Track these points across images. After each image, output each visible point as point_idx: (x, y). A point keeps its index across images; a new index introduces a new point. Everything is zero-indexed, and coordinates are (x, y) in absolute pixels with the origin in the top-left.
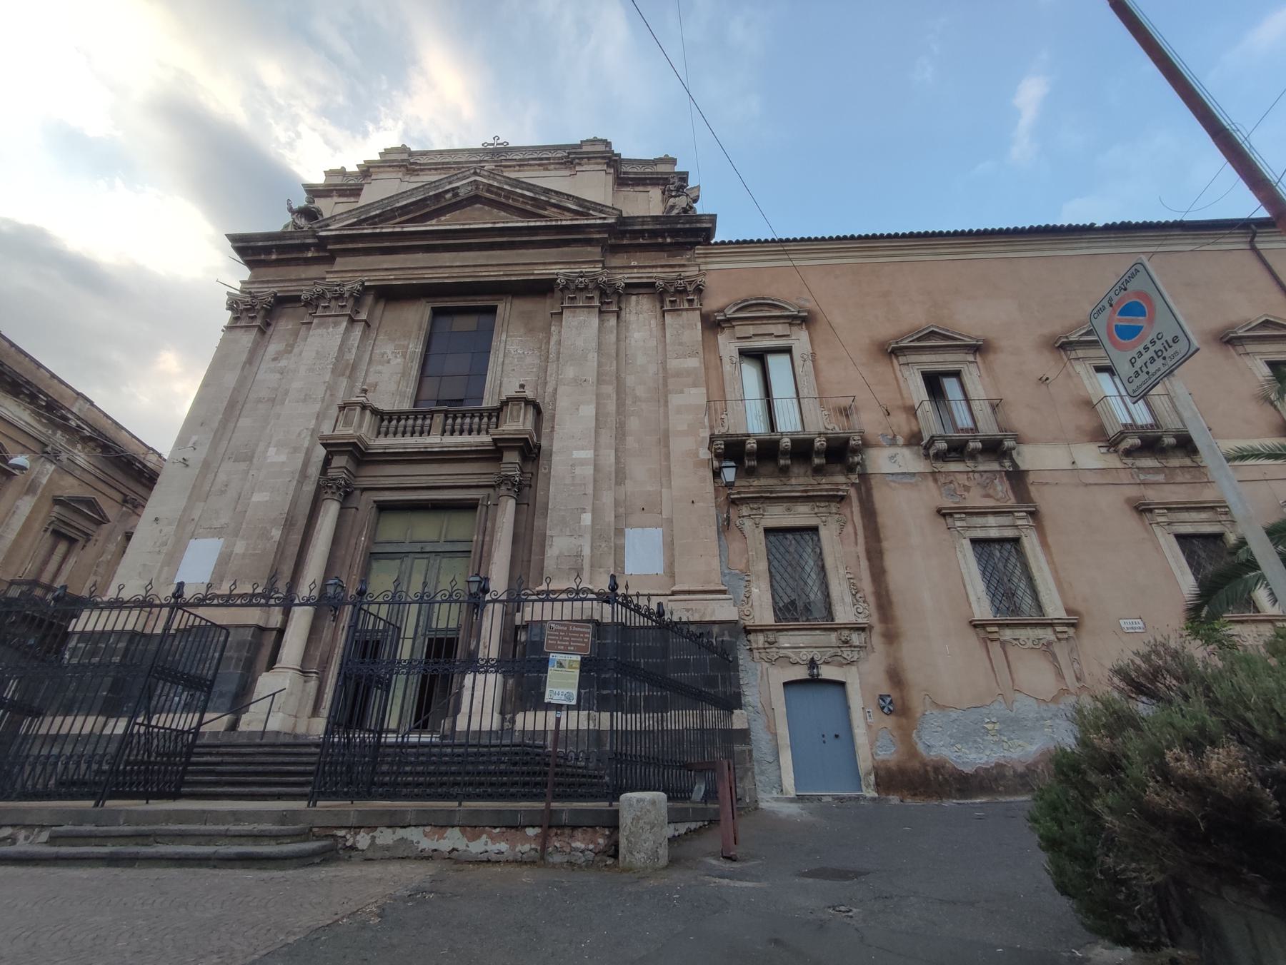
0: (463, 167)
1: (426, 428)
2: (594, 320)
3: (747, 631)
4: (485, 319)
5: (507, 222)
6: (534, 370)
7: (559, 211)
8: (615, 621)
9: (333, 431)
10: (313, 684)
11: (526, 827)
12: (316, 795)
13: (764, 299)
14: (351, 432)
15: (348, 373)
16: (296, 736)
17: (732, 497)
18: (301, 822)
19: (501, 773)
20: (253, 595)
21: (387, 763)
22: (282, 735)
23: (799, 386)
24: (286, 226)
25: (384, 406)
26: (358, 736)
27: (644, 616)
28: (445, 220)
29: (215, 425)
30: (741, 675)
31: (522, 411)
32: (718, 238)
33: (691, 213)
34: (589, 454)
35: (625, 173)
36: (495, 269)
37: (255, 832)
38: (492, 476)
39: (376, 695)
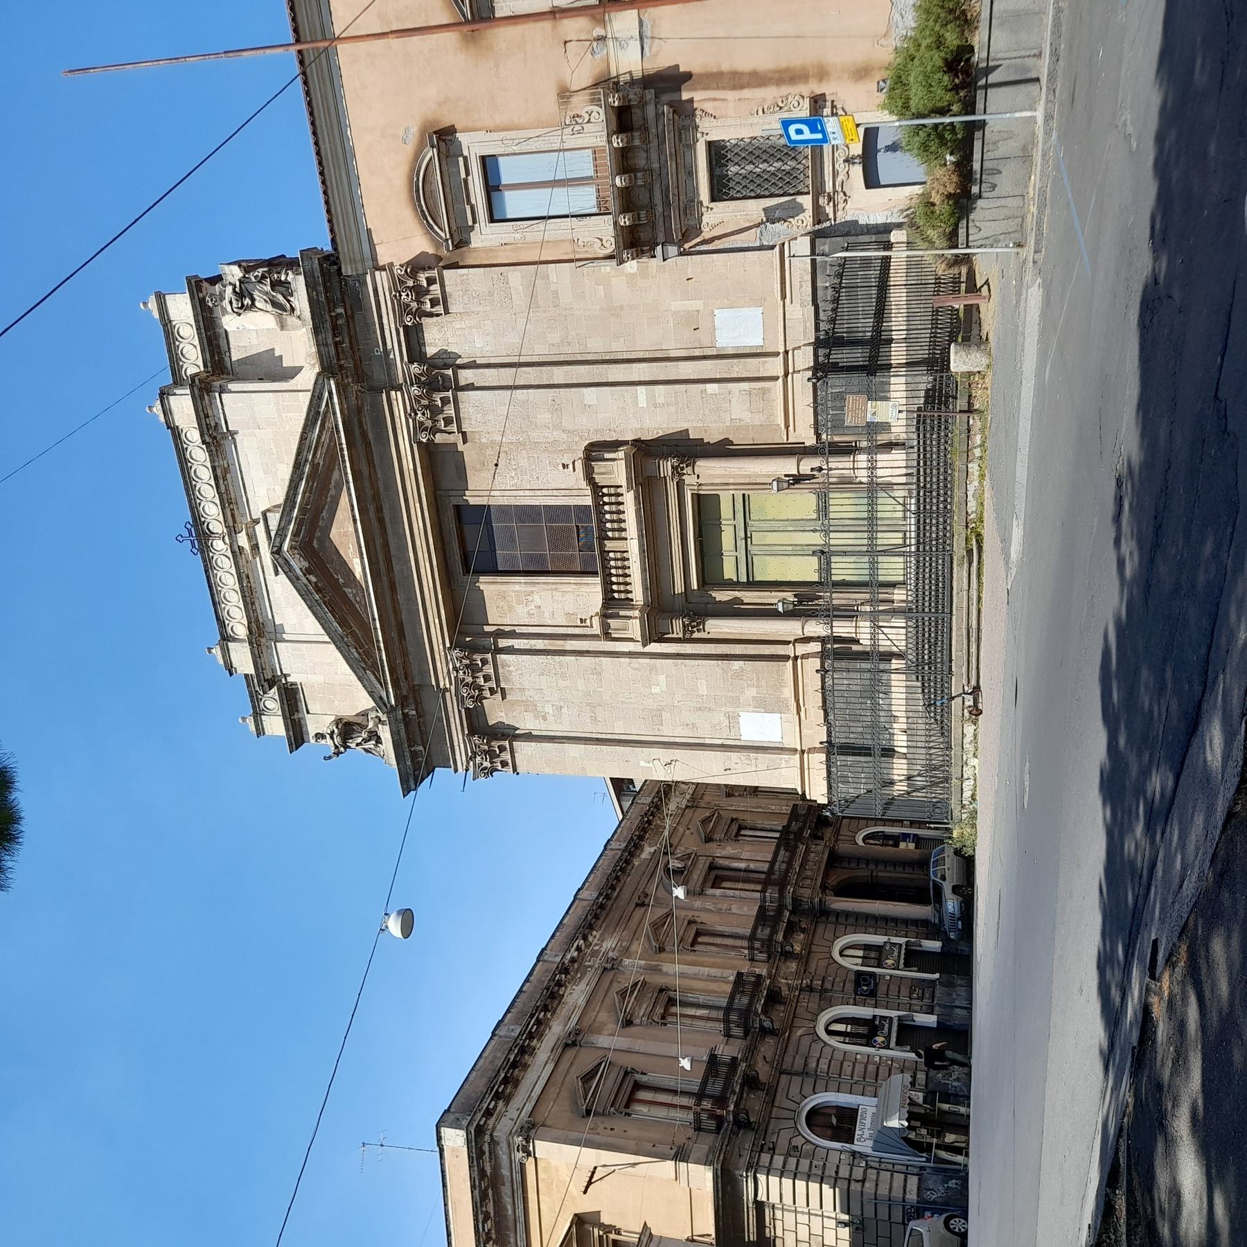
9: (638, 641)
32: (328, 248)
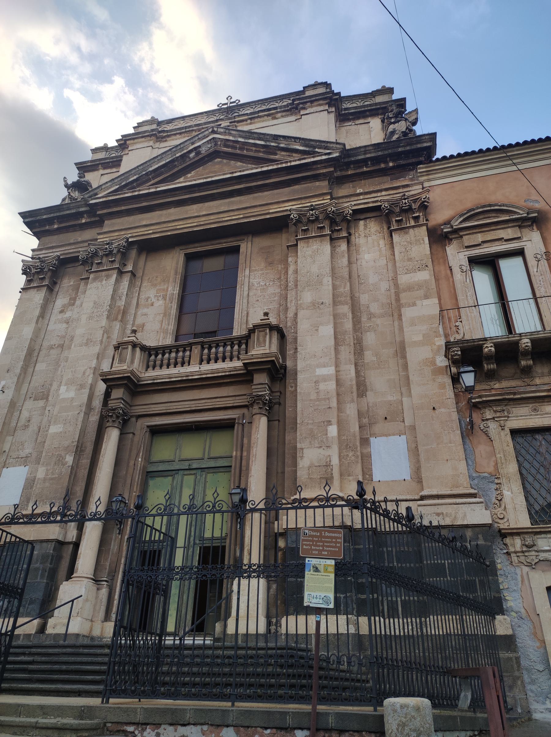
0: (203, 128)
1: (186, 359)
2: (326, 247)
3: (503, 535)
4: (230, 258)
5: (243, 171)
6: (276, 299)
7: (288, 154)
8: (366, 527)
9: (111, 368)
10: (104, 592)
11: (295, 729)
12: (108, 692)
13: (490, 205)
14: (125, 367)
15: (120, 317)
16: (92, 639)
17: (473, 401)
18: (97, 718)
19: (269, 675)
20: (51, 514)
21: (167, 664)
22: (81, 637)
23: (535, 286)
24: (64, 200)
25: (151, 342)
26: (140, 640)
27: (394, 520)
28: (191, 177)
29: (18, 371)
30: (501, 580)
31: (268, 337)
32: (439, 154)
33: (410, 135)
34: (331, 370)
35: (346, 109)
36: (236, 213)
37: (59, 725)
38: (245, 397)
39: (159, 599)
